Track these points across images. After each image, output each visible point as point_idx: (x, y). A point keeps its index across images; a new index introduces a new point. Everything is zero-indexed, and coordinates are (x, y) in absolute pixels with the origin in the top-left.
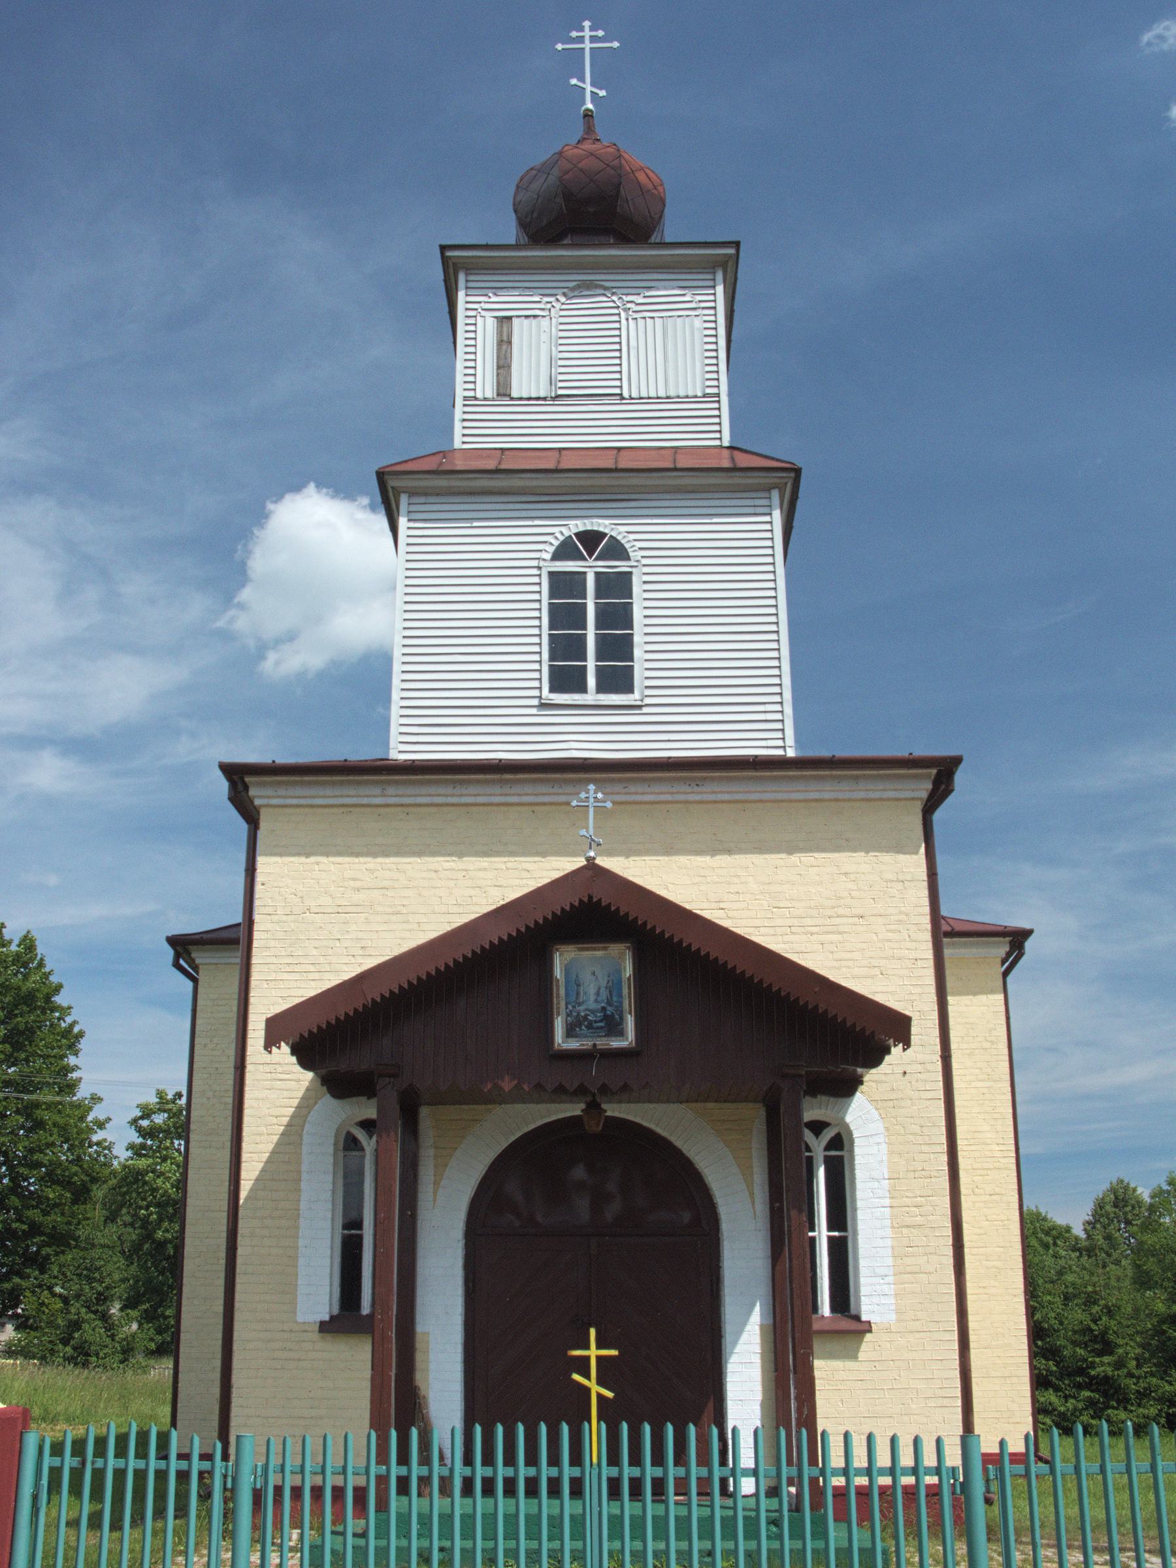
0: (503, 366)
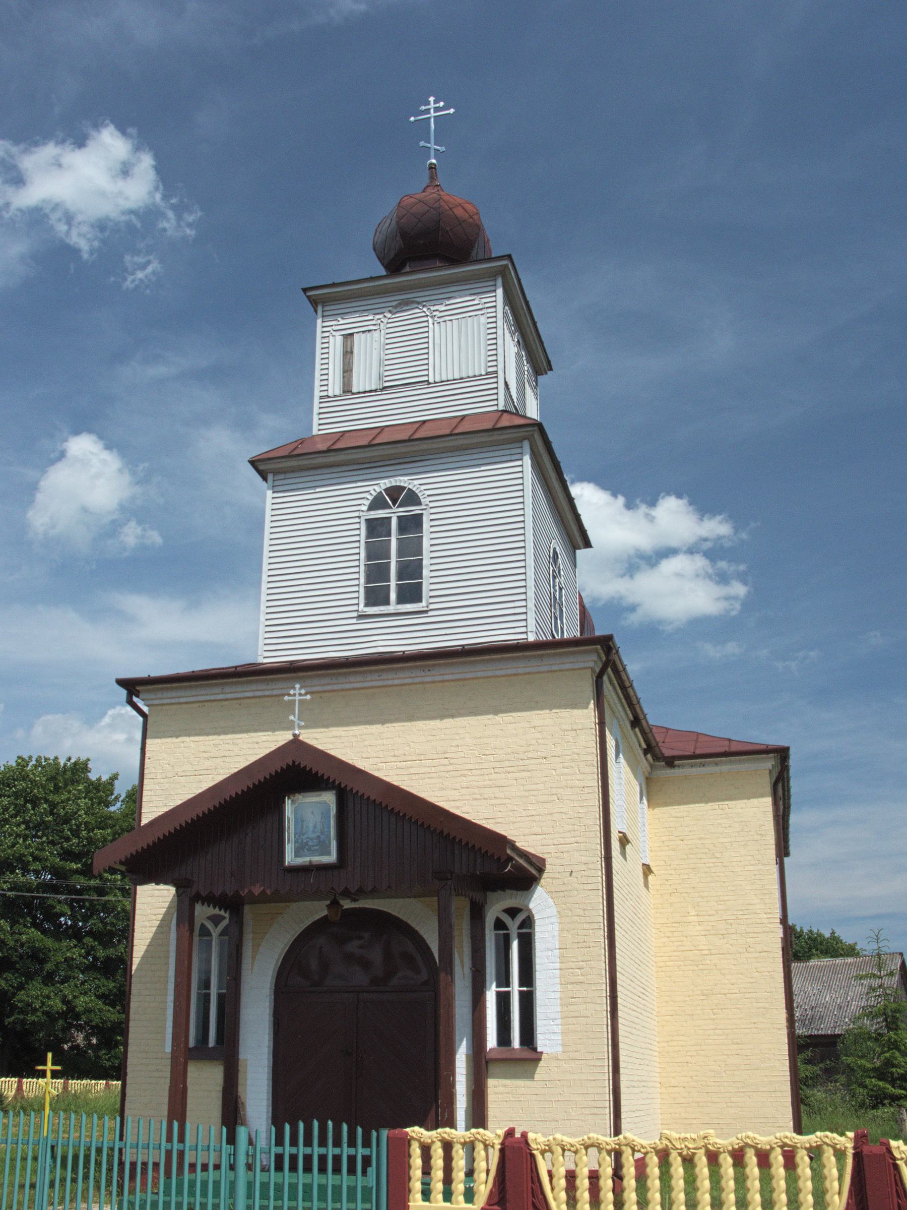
0: (347, 370)
